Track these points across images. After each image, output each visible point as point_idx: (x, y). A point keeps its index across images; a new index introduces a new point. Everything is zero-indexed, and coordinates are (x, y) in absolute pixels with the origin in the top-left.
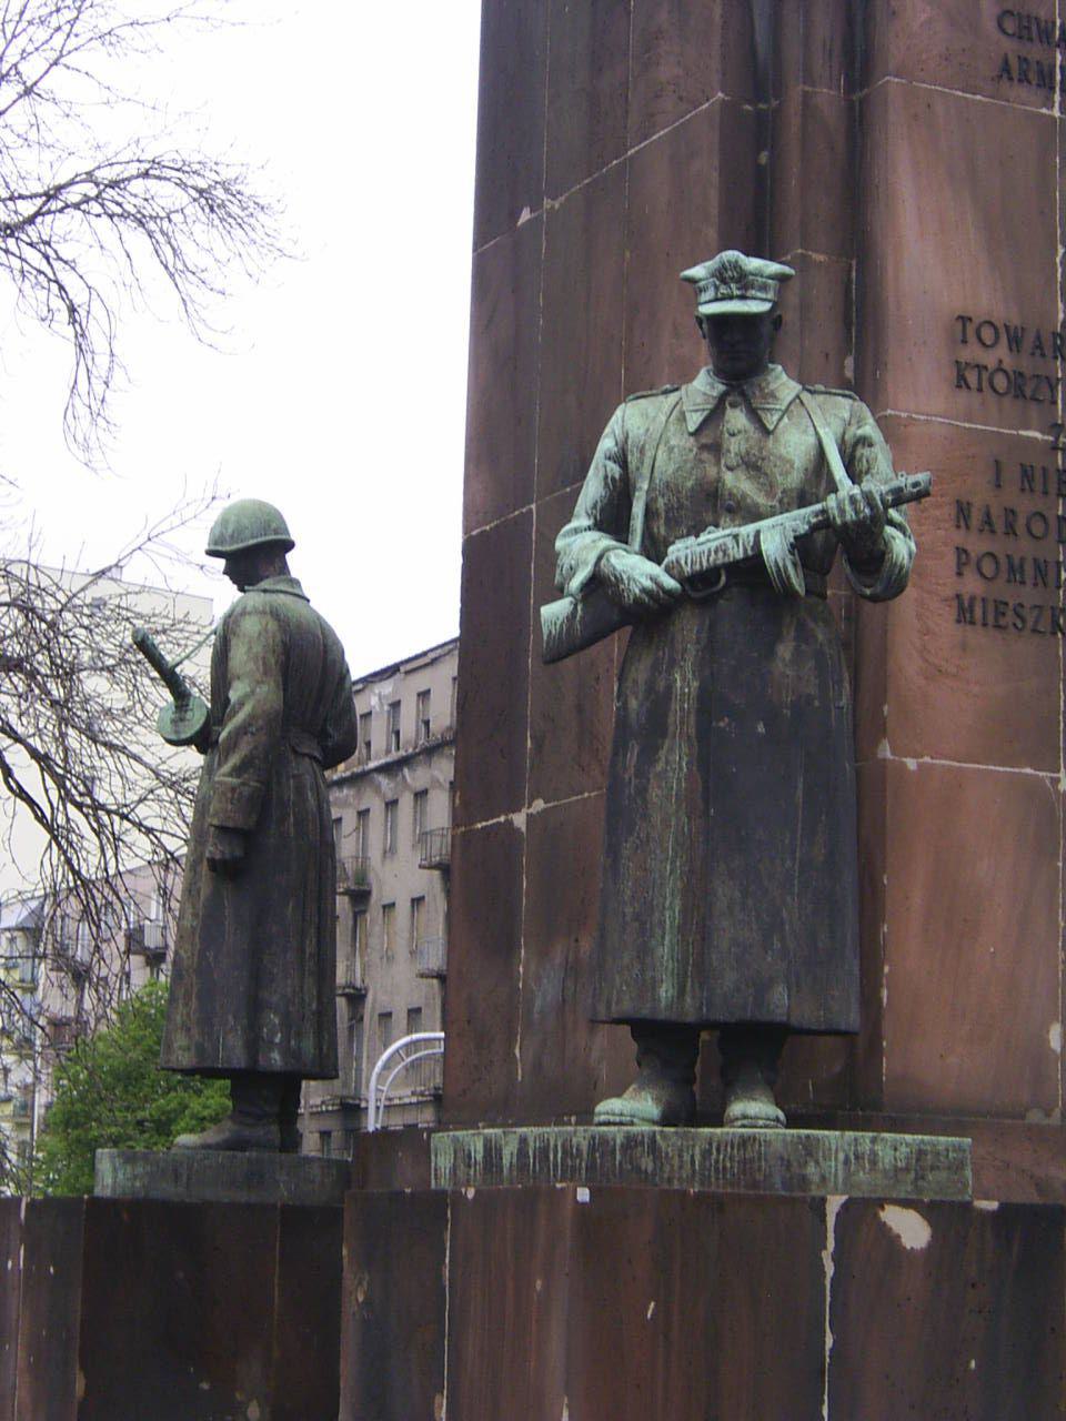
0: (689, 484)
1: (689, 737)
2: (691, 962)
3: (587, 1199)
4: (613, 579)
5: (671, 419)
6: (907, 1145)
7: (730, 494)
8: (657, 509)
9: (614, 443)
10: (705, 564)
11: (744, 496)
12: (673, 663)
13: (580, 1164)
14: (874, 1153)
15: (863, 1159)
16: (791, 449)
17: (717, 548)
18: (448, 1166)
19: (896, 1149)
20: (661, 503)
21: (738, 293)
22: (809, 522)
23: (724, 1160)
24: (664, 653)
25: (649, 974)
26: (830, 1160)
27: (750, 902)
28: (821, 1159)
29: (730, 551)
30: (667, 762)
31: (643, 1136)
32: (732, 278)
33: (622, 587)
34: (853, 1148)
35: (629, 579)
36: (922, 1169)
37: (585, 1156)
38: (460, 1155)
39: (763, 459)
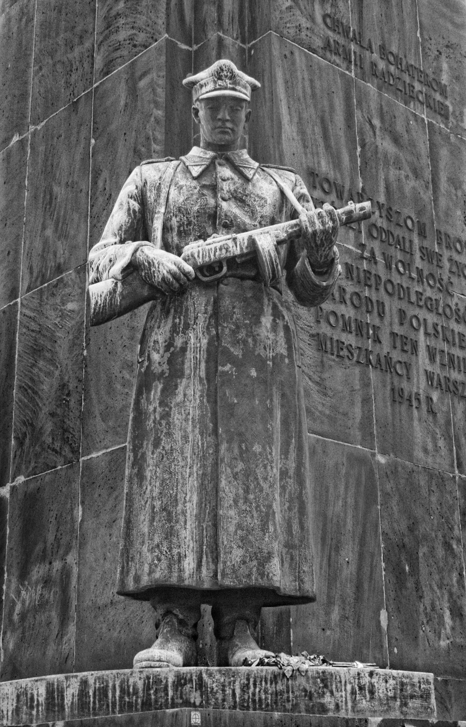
0: (196, 208)
1: (200, 377)
2: (205, 542)
3: (199, 721)
4: (146, 264)
5: (178, 170)
6: (394, 678)
7: (226, 215)
8: (171, 226)
9: (135, 187)
10: (212, 257)
11: (236, 217)
12: (187, 326)
13: (136, 701)
14: (372, 685)
15: (365, 690)
16: (264, 192)
17: (221, 246)
18: (11, 708)
19: (386, 682)
20: (174, 222)
21: (231, 86)
22: (287, 232)
23: (260, 692)
24: (180, 320)
25: (175, 551)
26: (341, 691)
27: (251, 497)
28: (334, 690)
29: (231, 249)
30: (185, 395)
31: (191, 675)
32: (226, 76)
33: (153, 269)
34: (357, 681)
35: (159, 264)
36: (405, 697)
37: (141, 694)
38: (23, 698)
39: (246, 196)
